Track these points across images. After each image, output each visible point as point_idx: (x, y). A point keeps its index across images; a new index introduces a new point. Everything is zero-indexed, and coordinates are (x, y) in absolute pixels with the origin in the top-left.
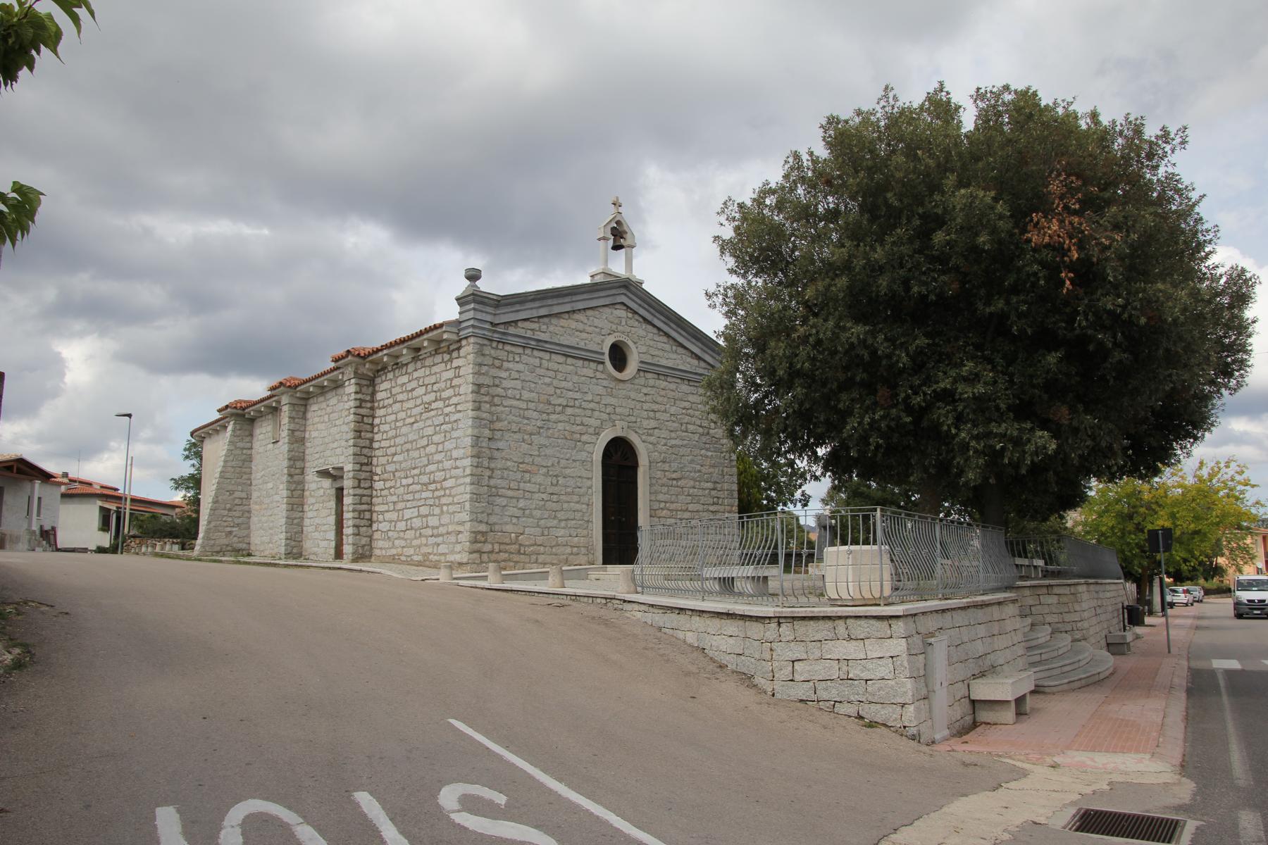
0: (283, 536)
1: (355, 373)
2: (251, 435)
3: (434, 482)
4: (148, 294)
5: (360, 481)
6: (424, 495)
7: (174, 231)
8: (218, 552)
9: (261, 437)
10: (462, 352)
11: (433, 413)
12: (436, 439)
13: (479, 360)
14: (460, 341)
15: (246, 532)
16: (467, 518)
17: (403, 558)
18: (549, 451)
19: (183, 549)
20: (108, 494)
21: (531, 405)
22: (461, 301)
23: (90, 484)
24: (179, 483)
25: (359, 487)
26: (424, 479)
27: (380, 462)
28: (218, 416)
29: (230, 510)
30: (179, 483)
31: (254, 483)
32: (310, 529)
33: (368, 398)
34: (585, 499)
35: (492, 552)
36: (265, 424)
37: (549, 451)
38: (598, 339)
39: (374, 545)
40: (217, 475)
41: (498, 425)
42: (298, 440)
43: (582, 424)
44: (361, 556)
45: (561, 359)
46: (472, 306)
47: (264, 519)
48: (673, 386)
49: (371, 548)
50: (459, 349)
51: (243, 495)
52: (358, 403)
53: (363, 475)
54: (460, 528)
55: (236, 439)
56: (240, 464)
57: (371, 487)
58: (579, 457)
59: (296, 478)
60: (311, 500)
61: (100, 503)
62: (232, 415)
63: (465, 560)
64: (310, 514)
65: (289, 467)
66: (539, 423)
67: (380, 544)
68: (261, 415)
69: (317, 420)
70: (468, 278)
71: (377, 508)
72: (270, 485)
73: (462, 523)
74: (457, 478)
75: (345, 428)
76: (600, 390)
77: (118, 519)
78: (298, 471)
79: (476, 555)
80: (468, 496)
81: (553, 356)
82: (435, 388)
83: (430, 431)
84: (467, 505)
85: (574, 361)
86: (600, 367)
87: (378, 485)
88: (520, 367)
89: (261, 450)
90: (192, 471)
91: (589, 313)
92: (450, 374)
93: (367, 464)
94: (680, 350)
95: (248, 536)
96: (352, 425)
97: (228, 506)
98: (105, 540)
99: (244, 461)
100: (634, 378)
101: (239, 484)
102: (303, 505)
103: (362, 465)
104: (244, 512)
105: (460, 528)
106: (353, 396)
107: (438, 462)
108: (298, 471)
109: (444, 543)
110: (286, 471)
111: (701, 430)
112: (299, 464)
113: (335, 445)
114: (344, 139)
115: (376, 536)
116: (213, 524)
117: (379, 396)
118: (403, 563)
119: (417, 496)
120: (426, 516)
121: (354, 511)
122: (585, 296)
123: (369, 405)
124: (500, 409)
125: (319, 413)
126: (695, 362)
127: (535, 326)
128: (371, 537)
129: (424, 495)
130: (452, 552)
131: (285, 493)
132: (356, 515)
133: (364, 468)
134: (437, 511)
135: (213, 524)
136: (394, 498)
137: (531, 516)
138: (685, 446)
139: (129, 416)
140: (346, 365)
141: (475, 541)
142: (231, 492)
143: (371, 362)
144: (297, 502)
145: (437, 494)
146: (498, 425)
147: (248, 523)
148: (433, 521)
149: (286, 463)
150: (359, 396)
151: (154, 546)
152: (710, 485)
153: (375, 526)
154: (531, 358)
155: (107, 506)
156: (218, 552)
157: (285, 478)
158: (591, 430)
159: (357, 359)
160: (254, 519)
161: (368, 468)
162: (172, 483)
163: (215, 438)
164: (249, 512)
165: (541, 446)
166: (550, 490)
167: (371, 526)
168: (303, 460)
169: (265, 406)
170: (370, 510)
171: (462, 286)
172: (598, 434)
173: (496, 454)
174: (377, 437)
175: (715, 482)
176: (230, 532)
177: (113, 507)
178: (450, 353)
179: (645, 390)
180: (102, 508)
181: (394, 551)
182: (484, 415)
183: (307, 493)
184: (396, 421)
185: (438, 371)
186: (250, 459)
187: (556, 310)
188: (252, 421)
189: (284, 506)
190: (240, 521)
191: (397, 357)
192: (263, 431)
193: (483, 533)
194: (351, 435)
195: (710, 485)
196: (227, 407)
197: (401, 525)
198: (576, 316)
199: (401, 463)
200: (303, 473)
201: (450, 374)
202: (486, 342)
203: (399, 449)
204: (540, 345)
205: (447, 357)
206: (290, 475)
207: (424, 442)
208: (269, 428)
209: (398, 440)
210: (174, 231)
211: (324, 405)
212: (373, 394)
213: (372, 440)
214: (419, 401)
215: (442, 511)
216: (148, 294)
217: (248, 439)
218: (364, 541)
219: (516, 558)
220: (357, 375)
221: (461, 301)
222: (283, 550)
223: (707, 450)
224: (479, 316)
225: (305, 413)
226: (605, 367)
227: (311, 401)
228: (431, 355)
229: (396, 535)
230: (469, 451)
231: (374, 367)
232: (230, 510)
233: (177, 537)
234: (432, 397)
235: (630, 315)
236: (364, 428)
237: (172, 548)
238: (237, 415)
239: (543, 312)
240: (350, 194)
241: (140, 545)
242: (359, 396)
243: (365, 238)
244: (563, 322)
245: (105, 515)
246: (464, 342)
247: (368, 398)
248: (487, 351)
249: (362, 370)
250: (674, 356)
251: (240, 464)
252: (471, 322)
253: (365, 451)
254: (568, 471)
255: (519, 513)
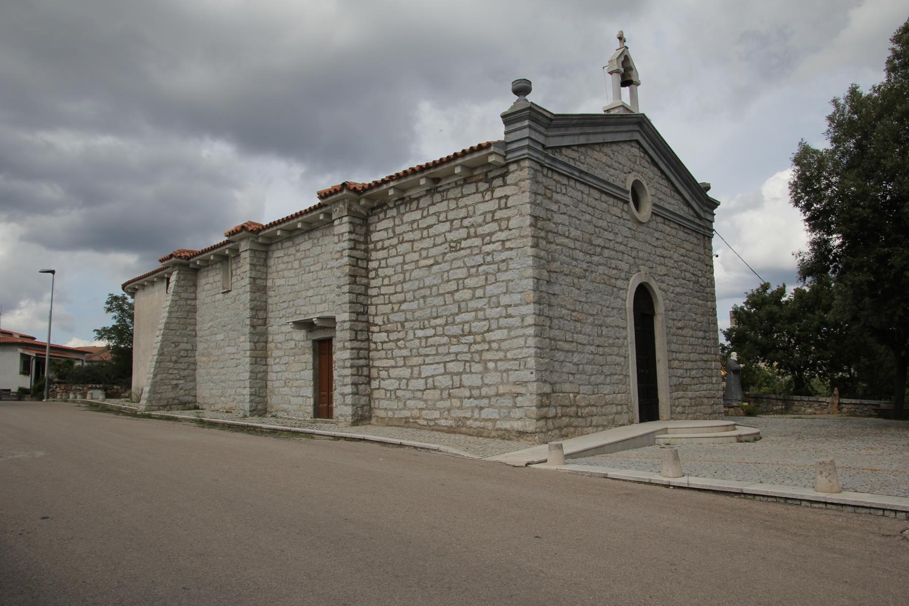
0: (247, 391)
1: (349, 210)
2: (195, 285)
3: (470, 333)
4: (49, 191)
5: (356, 332)
6: (454, 349)
7: (67, 144)
8: (165, 406)
9: (207, 287)
10: (510, 179)
11: (463, 252)
12: (470, 282)
13: (535, 187)
14: (507, 165)
15: (191, 384)
16: (533, 377)
17: (464, 429)
18: (594, 298)
19: (108, 396)
20: (27, 343)
21: (578, 244)
22: (508, 119)
23: (10, 334)
24: (103, 333)
25: (356, 339)
26: (455, 330)
27: (379, 311)
28: (160, 265)
29: (176, 362)
30: (103, 333)
31: (199, 334)
32: (277, 384)
33: (362, 239)
34: (623, 351)
35: (555, 417)
36: (211, 274)
37: (594, 298)
38: (622, 176)
39: (375, 404)
40: (162, 326)
41: (554, 266)
42: (259, 289)
43: (616, 268)
44: (362, 417)
45: (596, 194)
46: (526, 123)
47: (212, 371)
48: (674, 232)
49: (371, 409)
50: (504, 176)
51: (189, 347)
52: (352, 244)
53: (360, 326)
54: (522, 390)
55: (180, 290)
56: (184, 318)
57: (368, 340)
58: (615, 305)
59: (259, 329)
60: (276, 353)
61: (21, 350)
62: (174, 265)
63: (531, 428)
64: (276, 368)
65: (252, 317)
66: (585, 266)
67: (383, 406)
68: (207, 264)
69: (283, 266)
70: (516, 92)
71: (377, 363)
72: (220, 337)
73: (524, 383)
74: (509, 328)
75: (338, 273)
76: (628, 233)
77: (38, 364)
78: (260, 322)
79: (542, 423)
80: (532, 351)
81: (593, 192)
82: (466, 222)
83: (461, 273)
84: (531, 362)
85: (608, 198)
86: (626, 207)
87: (379, 337)
88: (566, 200)
89: (208, 300)
90: (114, 322)
91: (615, 147)
92: (493, 205)
93: (363, 314)
94: (676, 196)
95: (194, 388)
96: (347, 269)
97: (174, 358)
98: (26, 382)
99: (188, 312)
100: (649, 221)
101: (184, 336)
102: (266, 358)
103: (358, 314)
104: (189, 364)
105: (522, 390)
106: (347, 236)
107: (476, 310)
108: (260, 322)
109: (490, 406)
110: (248, 322)
111: (693, 278)
112: (261, 314)
113: (310, 293)
114: (195, 78)
115: (376, 394)
116: (159, 377)
117: (375, 237)
118: (422, 427)
119: (442, 350)
120: (459, 374)
121: (352, 367)
122: (611, 129)
123: (363, 247)
124: (553, 247)
125: (286, 259)
126: (686, 208)
127: (575, 155)
128: (370, 396)
129: (454, 349)
130: (507, 418)
131: (248, 345)
132: (354, 371)
133: (361, 318)
134: (477, 368)
135: (159, 377)
136: (405, 352)
137: (583, 372)
138: (684, 294)
139: (53, 272)
140: (336, 201)
141: (541, 406)
142: (177, 344)
143: (367, 198)
144: (260, 355)
145: (474, 348)
146: (554, 266)
147: (194, 376)
148: (467, 380)
149: (248, 313)
150: (353, 236)
151: (84, 395)
152: (701, 334)
153: (375, 384)
154: (577, 191)
155: (27, 353)
156: (165, 406)
157: (247, 329)
158: (623, 275)
159: (351, 194)
160: (201, 373)
161: (364, 318)
162: (95, 334)
163: (149, 290)
164: (195, 364)
165: (589, 292)
166: (597, 342)
167: (369, 383)
168: (265, 310)
169: (215, 255)
170: (368, 366)
171: (508, 102)
172: (628, 279)
173: (554, 300)
174: (373, 283)
175: (705, 331)
176: (177, 385)
177: (33, 354)
178: (489, 181)
179: (657, 235)
180: (22, 355)
181: (407, 413)
182: (543, 253)
183: (271, 346)
184: (404, 263)
185: (477, 203)
186: (194, 309)
187: (593, 139)
188: (196, 271)
189: (248, 360)
190: (186, 373)
191: (404, 191)
192: (210, 283)
193: (547, 395)
194: (347, 280)
195: (701, 334)
196: (171, 256)
197: (414, 384)
198: (606, 150)
199: (413, 311)
200: (265, 324)
201: (493, 205)
202: (539, 168)
203: (409, 296)
204: (582, 178)
205: (483, 186)
206: (253, 326)
207: (453, 286)
208: (219, 277)
209: (407, 286)
210: (67, 144)
211: (292, 250)
212: (368, 234)
213: (367, 286)
214: (439, 240)
215: (486, 369)
216: (49, 191)
217: (192, 289)
218: (364, 400)
219: (576, 422)
220: (351, 213)
221: (508, 119)
222: (247, 407)
223: (698, 298)
224: (535, 136)
225: (266, 260)
226: (629, 207)
227: (274, 247)
228: (457, 186)
229: (408, 394)
230: (531, 296)
231: (370, 204)
232: (176, 362)
233: (99, 383)
234: (463, 233)
235: (642, 155)
236: (359, 273)
237: (97, 396)
238: (181, 265)
239: (582, 140)
240: (202, 119)
241: (67, 392)
242: (353, 236)
243: (216, 152)
244: (596, 155)
245: (26, 362)
246: (512, 167)
247: (362, 239)
248: (540, 178)
249: (355, 207)
250: (673, 201)
251: (184, 318)
252: (526, 142)
253: (361, 299)
254: (608, 320)
255: (574, 369)
